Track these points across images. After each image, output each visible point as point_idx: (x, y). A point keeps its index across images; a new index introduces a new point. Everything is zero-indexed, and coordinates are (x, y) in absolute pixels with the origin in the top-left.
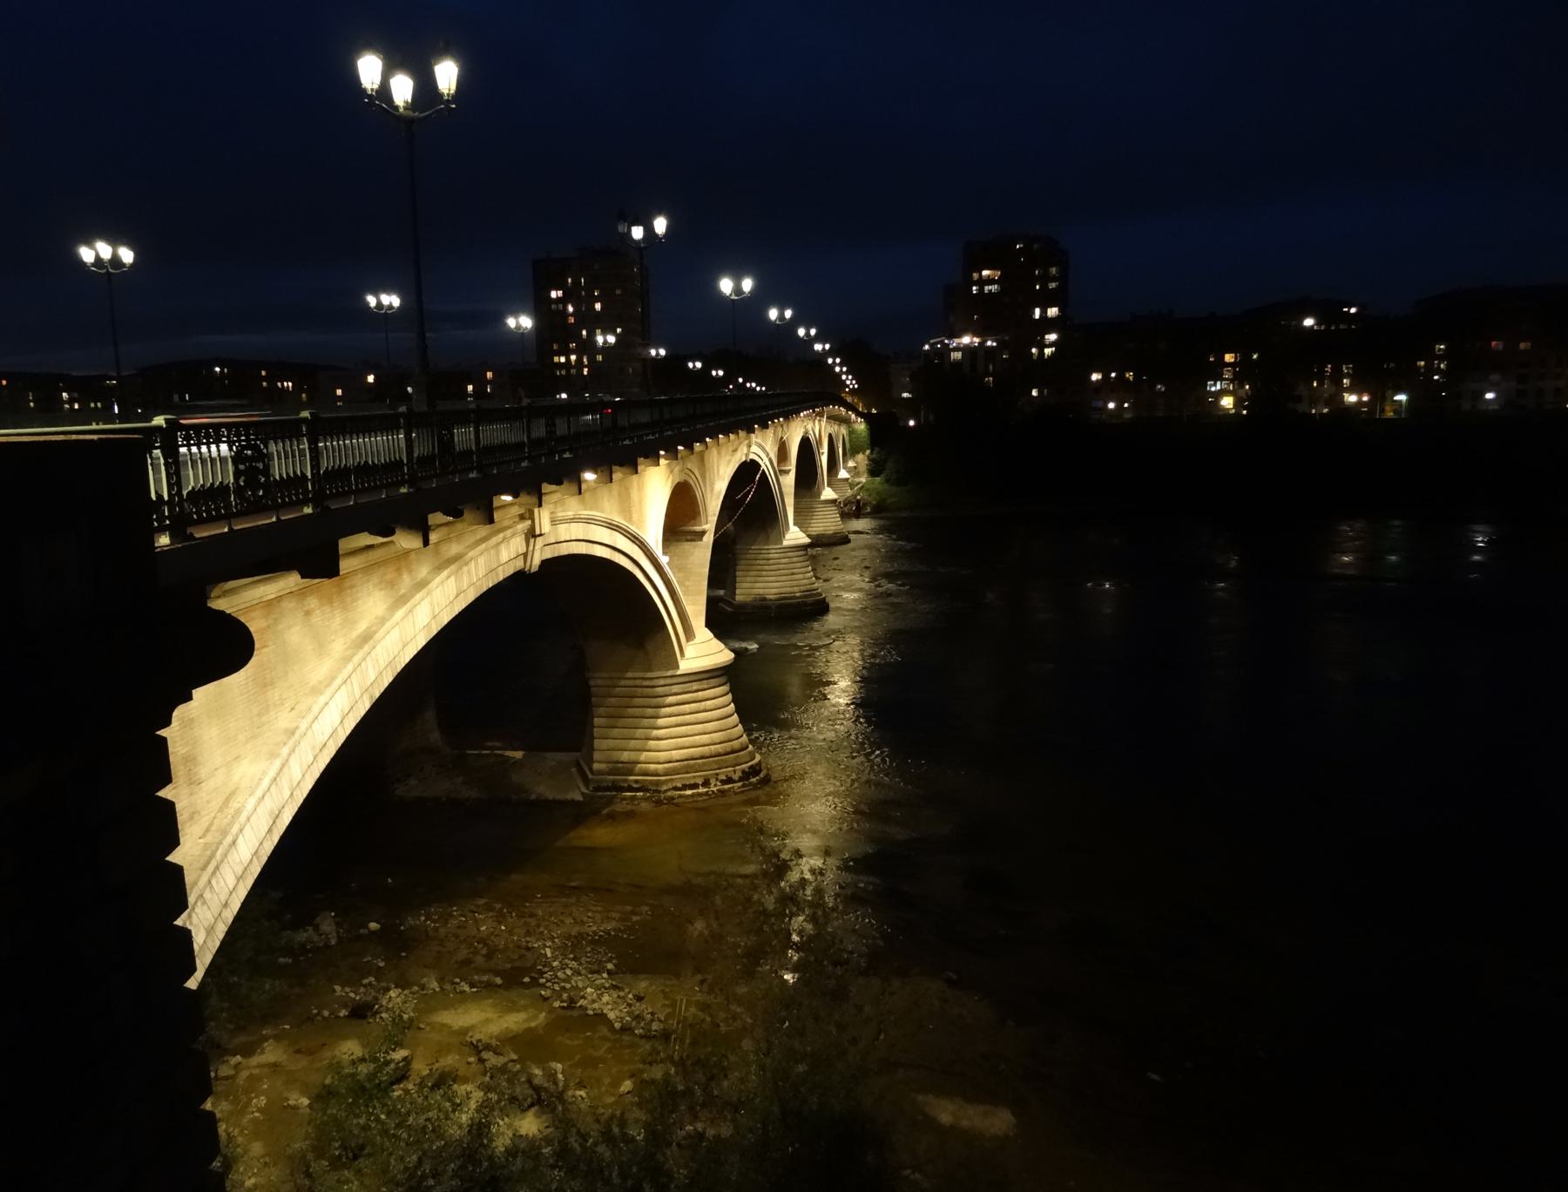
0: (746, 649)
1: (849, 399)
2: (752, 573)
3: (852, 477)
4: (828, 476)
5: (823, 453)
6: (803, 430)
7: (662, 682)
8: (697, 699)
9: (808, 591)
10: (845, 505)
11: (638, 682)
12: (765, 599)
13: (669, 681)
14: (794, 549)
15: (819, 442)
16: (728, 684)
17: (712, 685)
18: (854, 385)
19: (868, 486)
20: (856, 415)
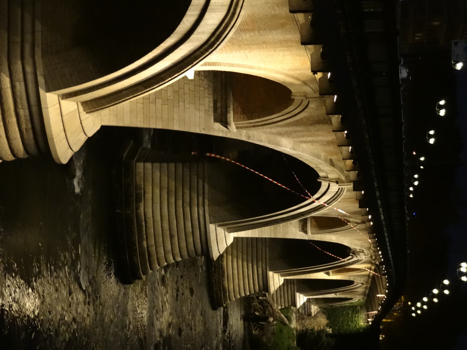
0: (74, 176)
1: (397, 306)
2: (173, 183)
3: (298, 310)
4: (298, 280)
5: (328, 274)
6: (358, 248)
7: (29, 69)
8: (6, 115)
9: (149, 255)
10: (261, 302)
11: (28, 37)
12: (138, 200)
13: (30, 77)
14: (203, 238)
15: (342, 269)
16: (26, 156)
17: (25, 136)
18: (415, 312)
19: (285, 331)
20: (376, 315)
